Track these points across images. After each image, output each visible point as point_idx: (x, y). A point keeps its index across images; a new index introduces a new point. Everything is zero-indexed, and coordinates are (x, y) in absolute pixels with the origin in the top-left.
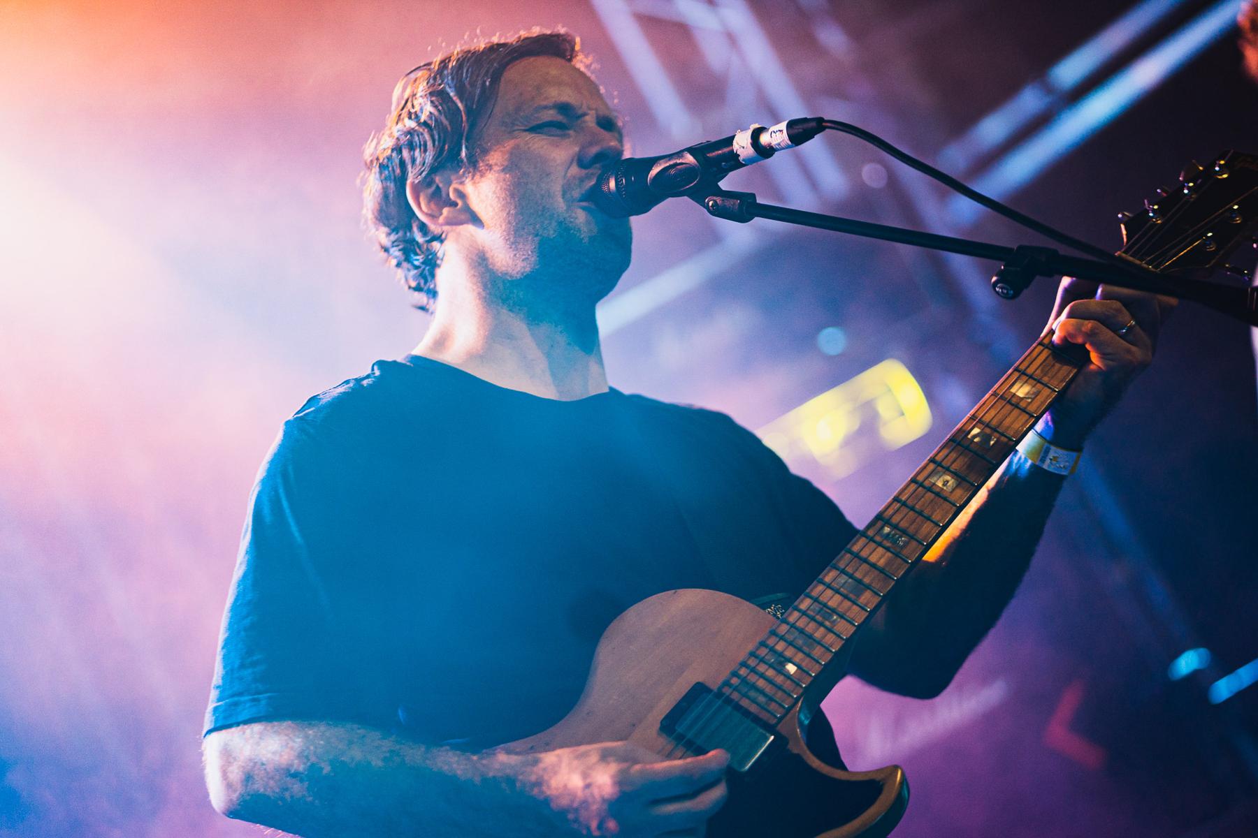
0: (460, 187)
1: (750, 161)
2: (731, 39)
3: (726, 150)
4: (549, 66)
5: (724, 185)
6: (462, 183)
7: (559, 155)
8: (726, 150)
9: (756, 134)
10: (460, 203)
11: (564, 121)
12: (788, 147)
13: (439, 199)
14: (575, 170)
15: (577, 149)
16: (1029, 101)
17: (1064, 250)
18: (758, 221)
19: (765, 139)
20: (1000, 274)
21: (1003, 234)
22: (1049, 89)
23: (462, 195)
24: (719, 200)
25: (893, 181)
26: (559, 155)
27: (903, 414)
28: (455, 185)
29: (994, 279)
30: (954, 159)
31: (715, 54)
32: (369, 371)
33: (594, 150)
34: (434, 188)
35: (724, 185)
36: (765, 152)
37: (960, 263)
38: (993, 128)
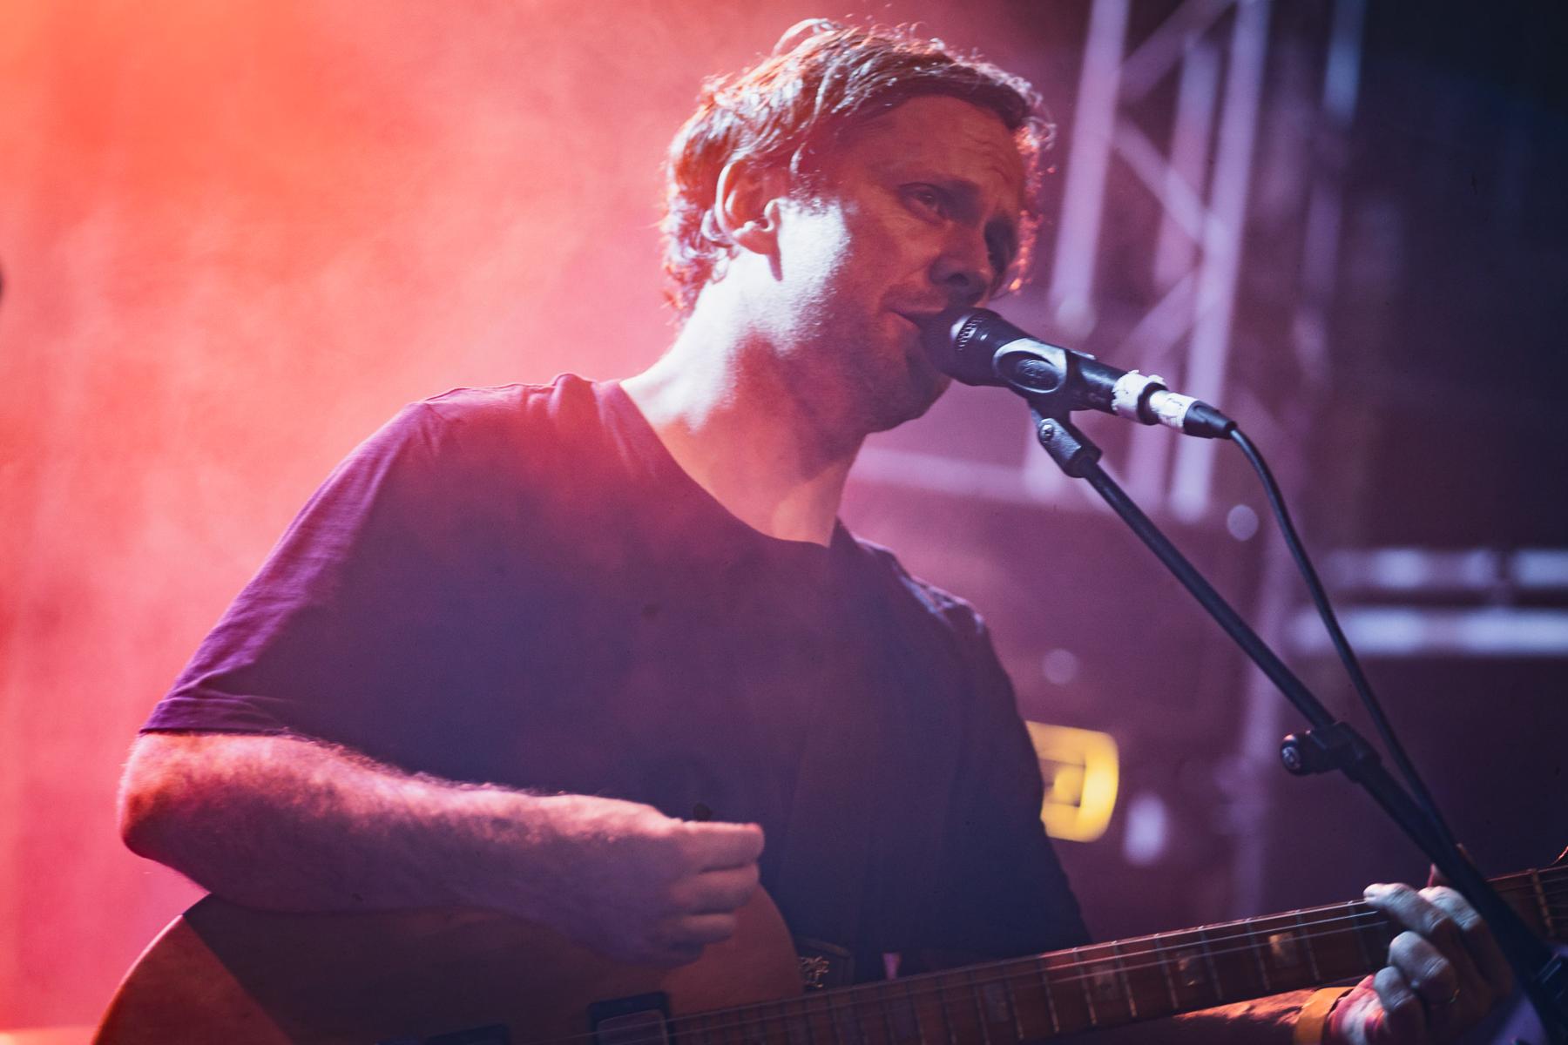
0: (782, 208)
1: (1123, 413)
2: (1198, 256)
3: (1105, 380)
4: (976, 126)
5: (1075, 417)
6: (788, 206)
7: (917, 245)
8: (1105, 380)
9: (1152, 388)
10: (770, 228)
11: (945, 200)
12: (1174, 429)
13: (749, 208)
14: (918, 278)
15: (937, 250)
16: (1475, 568)
17: (1388, 763)
18: (1083, 484)
19: (1158, 401)
20: (1301, 737)
21: (1327, 686)
22: (1503, 571)
23: (776, 215)
24: (1059, 430)
25: (1258, 542)
26: (917, 245)
27: (1077, 804)
28: (781, 201)
29: (1290, 738)
30: (1343, 569)
31: (1169, 260)
32: (549, 385)
33: (956, 266)
34: (757, 186)
35: (1075, 417)
36: (1145, 414)
37: (1263, 689)
38: (1402, 568)
